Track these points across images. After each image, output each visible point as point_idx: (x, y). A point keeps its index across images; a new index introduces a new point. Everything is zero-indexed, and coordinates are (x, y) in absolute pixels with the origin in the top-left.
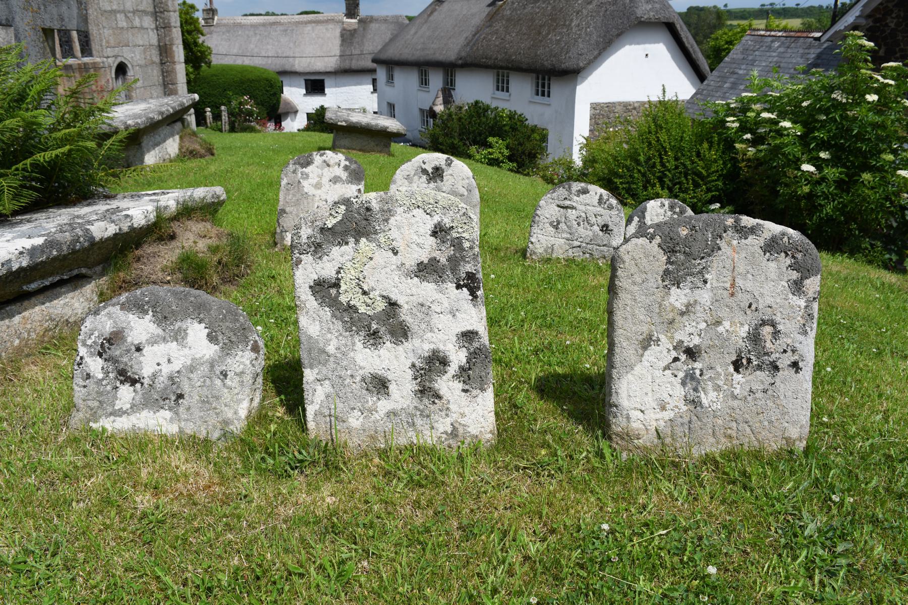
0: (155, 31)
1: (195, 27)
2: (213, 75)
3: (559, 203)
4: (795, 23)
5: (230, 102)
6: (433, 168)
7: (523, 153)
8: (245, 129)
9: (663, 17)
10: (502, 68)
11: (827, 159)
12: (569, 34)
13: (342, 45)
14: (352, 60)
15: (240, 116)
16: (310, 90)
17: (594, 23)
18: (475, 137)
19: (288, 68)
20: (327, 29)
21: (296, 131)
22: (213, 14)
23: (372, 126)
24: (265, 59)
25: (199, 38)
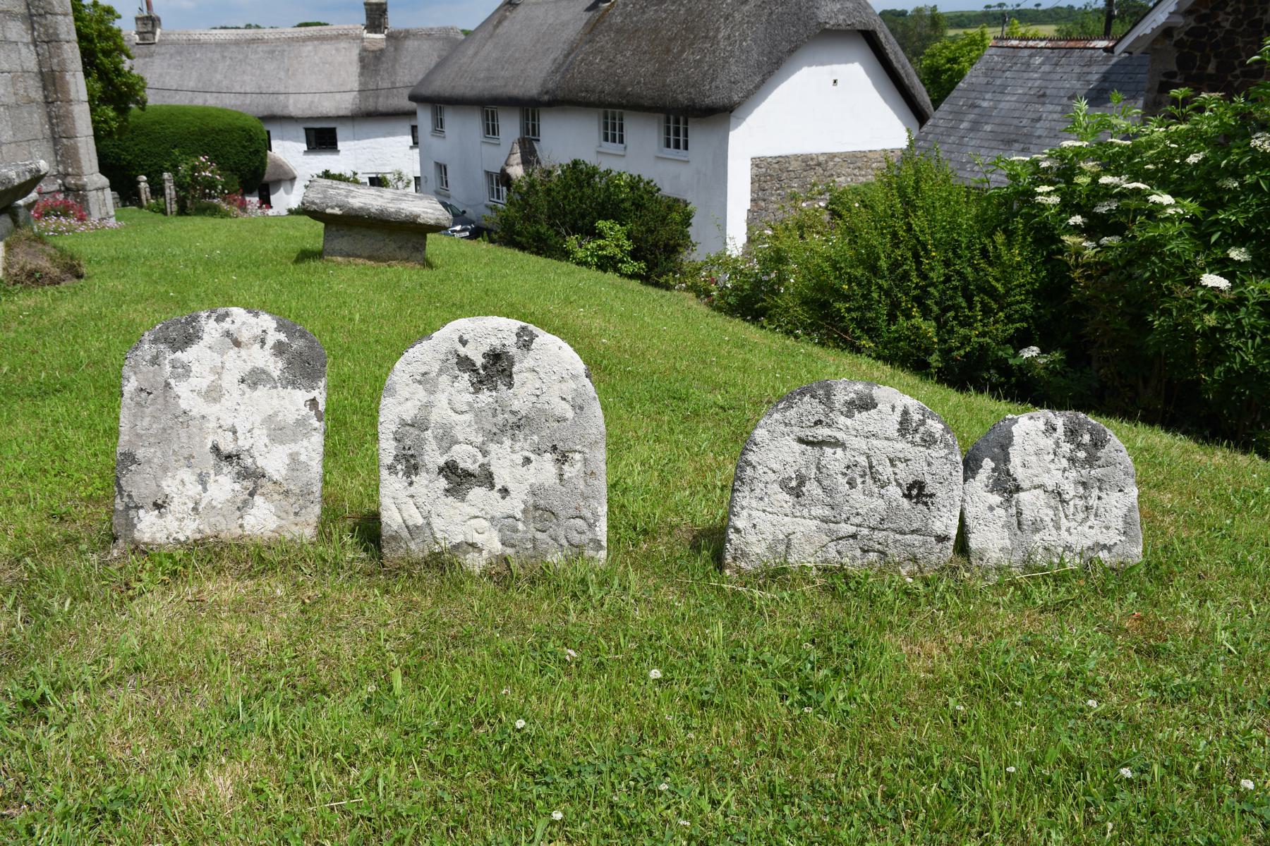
0: (32, 48)
1: (115, 43)
2: (154, 123)
3: (802, 435)
4: (1049, 30)
5: (177, 166)
6: (485, 355)
7: (656, 245)
8: (203, 211)
9: (858, 22)
10: (611, 105)
11: (1245, 262)
12: (714, 52)
13: (361, 74)
14: (378, 97)
15: (195, 190)
16: (313, 144)
17: (753, 33)
18: (576, 221)
19: (277, 111)
20: (337, 50)
21: (285, 213)
22: (153, 26)
23: (391, 213)
24: (241, 97)
25: (123, 62)
